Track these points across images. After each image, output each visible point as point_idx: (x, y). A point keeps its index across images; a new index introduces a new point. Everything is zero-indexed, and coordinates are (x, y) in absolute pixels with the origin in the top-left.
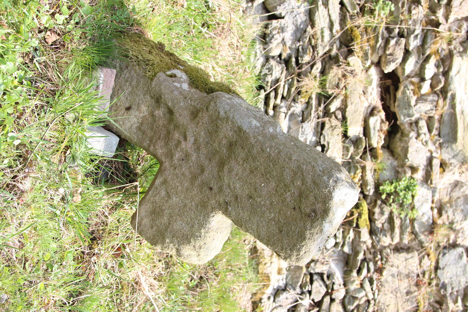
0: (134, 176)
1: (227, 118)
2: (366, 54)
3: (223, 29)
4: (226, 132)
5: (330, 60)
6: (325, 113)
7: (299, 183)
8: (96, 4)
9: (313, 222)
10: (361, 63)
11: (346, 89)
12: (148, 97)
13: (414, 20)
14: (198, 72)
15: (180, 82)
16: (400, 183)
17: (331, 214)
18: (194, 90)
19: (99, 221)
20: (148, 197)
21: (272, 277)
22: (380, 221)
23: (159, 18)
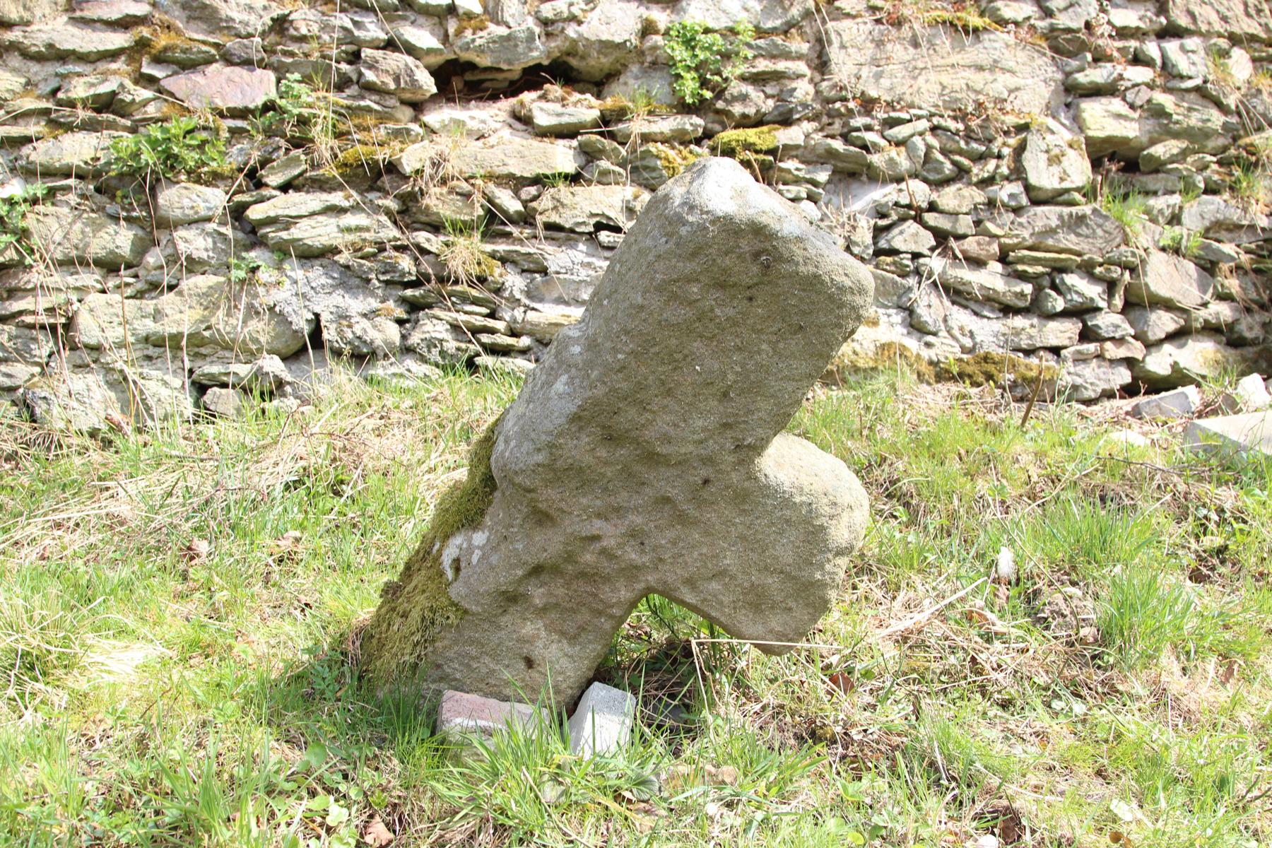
0: (675, 649)
1: (551, 447)
2: (397, 134)
3: (344, 449)
4: (581, 449)
5: (410, 213)
6: (526, 223)
7: (695, 290)
8: (303, 735)
9: (780, 259)
10: (417, 146)
11: (472, 177)
12: (504, 620)
13: (322, 29)
14: (447, 510)
15: (470, 550)
16: (679, 58)
17: (764, 220)
18: (487, 518)
19: (772, 726)
20: (722, 619)
21: (884, 339)
22: (760, 103)
23: (327, 592)
